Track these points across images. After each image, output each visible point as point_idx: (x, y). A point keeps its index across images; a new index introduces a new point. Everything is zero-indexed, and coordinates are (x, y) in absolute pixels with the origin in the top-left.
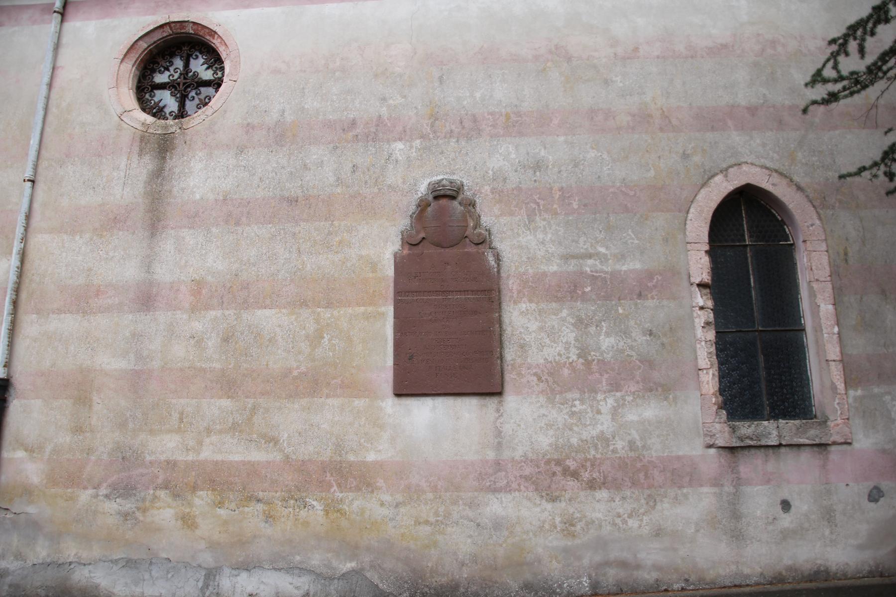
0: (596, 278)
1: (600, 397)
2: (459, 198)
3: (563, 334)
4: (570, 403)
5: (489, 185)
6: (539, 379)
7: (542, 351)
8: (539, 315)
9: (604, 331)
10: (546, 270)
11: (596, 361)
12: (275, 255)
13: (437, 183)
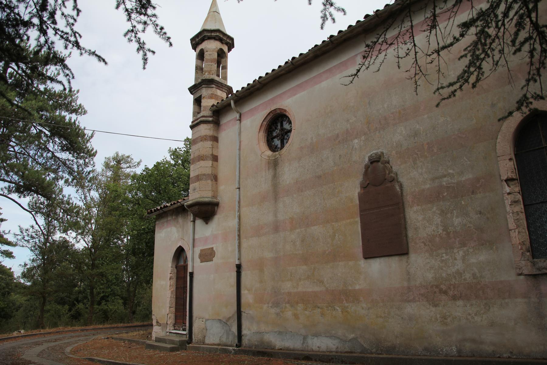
2: (381, 161)
4: (441, 255)
6: (425, 244)
11: (452, 232)
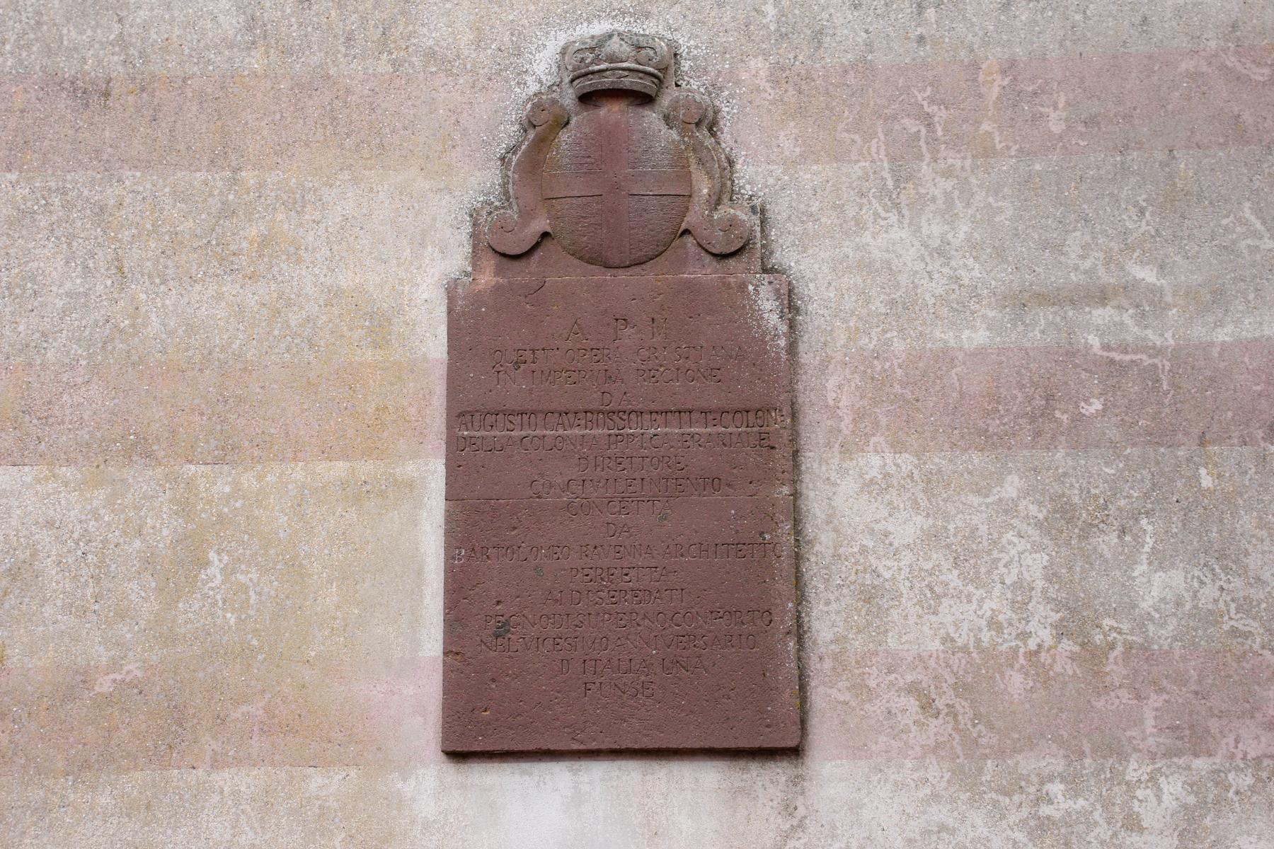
0: (1123, 369)
1: (1135, 770)
2: (665, 101)
3: (1005, 558)
4: (1032, 789)
5: (766, 54)
6: (927, 705)
7: (935, 613)
8: (925, 491)
9: (1147, 549)
10: (952, 343)
11: (1119, 649)
12: (33, 279)
13: (592, 49)
